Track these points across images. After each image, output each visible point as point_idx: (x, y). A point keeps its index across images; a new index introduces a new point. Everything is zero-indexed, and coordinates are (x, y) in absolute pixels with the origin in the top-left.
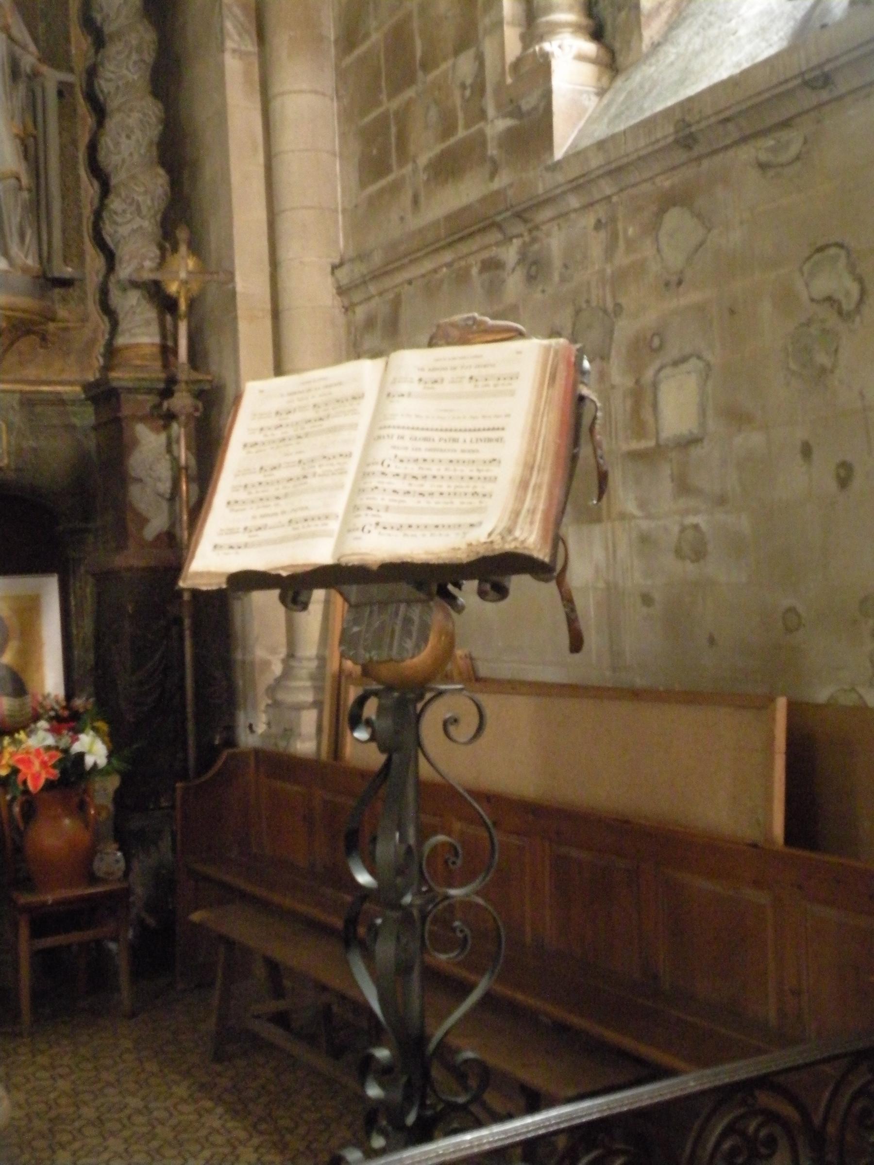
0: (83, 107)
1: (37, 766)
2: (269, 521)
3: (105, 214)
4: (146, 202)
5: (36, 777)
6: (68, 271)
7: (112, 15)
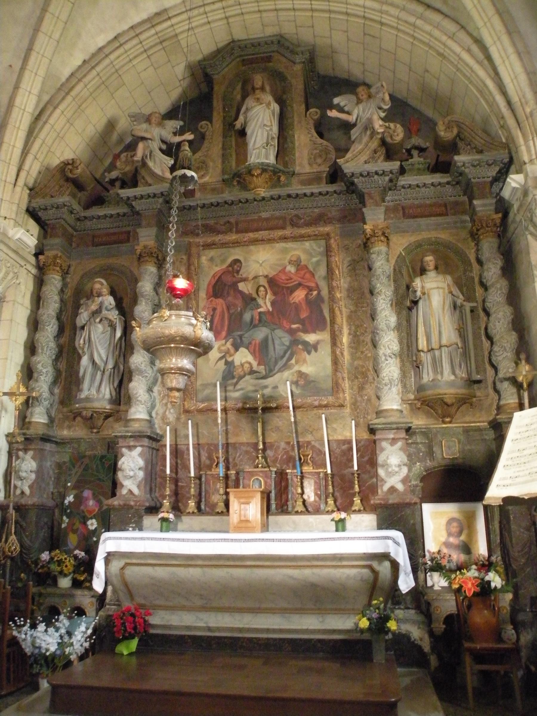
0: (482, 314)
1: (470, 585)
2: (521, 474)
3: (492, 353)
4: (508, 346)
5: (470, 590)
6: (478, 377)
7: (490, 279)
